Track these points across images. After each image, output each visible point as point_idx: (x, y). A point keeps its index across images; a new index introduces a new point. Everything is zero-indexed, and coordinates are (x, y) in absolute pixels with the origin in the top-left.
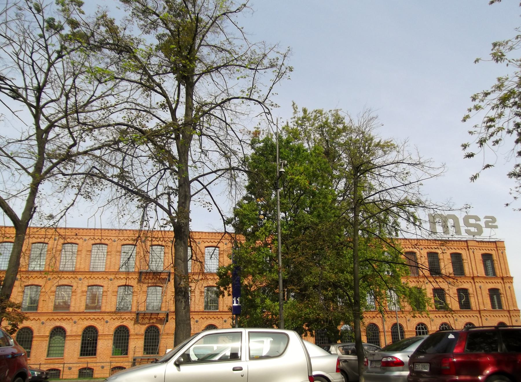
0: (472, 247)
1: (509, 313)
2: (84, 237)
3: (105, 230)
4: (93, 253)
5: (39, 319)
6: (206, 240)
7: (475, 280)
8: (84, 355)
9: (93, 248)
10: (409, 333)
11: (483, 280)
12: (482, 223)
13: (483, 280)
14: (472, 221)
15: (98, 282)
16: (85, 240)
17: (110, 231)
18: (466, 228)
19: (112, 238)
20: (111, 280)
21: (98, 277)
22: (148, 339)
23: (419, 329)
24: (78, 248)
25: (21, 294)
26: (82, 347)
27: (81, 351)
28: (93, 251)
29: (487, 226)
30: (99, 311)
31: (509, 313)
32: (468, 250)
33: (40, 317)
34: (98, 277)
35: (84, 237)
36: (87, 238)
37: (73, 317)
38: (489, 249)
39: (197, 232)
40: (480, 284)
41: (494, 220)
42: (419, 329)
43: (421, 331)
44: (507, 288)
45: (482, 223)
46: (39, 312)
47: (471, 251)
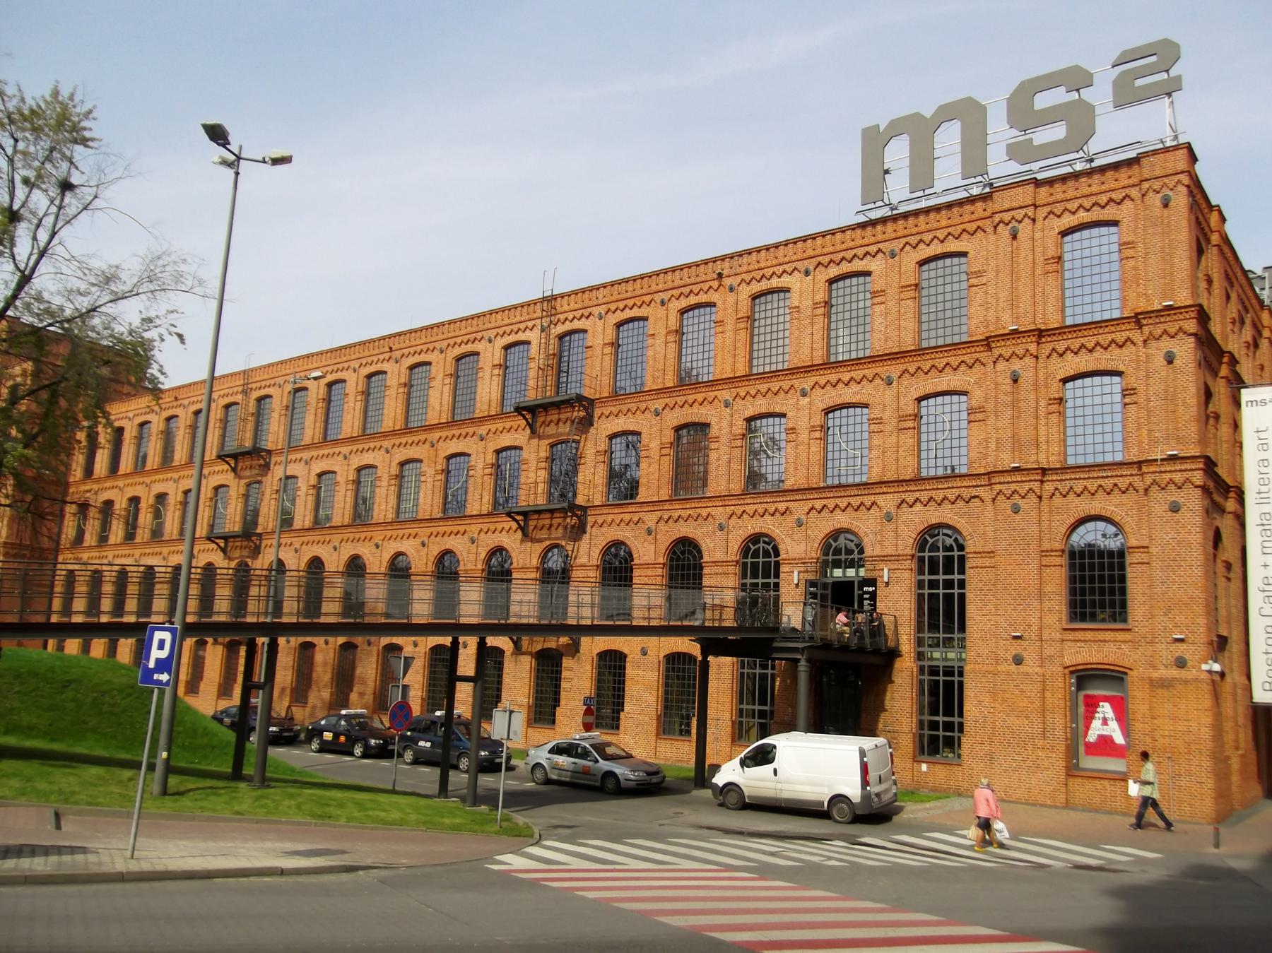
29: (1126, 96)
36: (810, 264)
41: (1166, 53)
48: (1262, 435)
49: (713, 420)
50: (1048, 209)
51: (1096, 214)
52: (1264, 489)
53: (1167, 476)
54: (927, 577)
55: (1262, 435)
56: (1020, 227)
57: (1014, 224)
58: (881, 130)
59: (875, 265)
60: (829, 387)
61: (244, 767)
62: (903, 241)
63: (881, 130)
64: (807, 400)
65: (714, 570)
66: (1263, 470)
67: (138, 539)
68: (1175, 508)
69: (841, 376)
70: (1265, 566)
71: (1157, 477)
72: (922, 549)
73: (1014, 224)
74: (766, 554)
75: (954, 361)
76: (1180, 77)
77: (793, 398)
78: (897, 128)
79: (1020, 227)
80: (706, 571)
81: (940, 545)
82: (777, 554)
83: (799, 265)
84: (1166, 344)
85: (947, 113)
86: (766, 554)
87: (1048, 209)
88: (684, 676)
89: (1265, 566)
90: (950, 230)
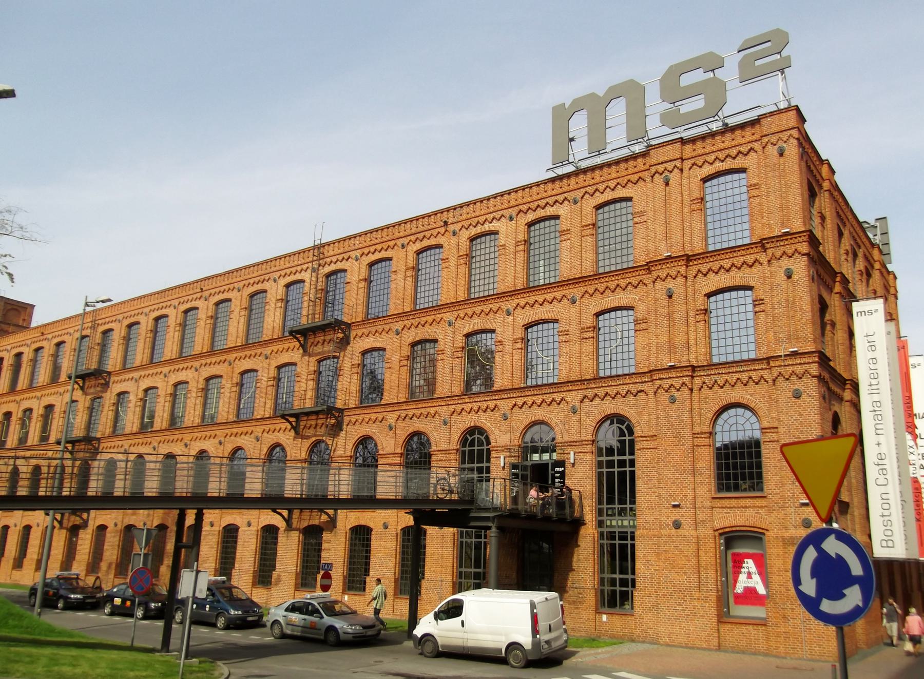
2: (353, 254)
3: (329, 244)
4: (709, 205)
5: (562, 399)
8: (728, 489)
9: (708, 191)
10: (440, 457)
12: (729, 73)
15: (621, 299)
16: (575, 202)
17: (458, 211)
19: (742, 149)
21: (722, 267)
23: (472, 444)
24: (748, 178)
25: (590, 334)
26: (759, 466)
27: (719, 477)
28: (708, 198)
33: (498, 402)
34: (722, 267)
36: (513, 212)
37: (567, 396)
48: (870, 339)
49: (440, 337)
55: (870, 339)
56: (671, 176)
57: (666, 173)
62: (583, 190)
64: (511, 318)
73: (666, 173)
78: (578, 106)
79: (671, 176)
83: (505, 213)
84: (785, 263)
85: (615, 93)
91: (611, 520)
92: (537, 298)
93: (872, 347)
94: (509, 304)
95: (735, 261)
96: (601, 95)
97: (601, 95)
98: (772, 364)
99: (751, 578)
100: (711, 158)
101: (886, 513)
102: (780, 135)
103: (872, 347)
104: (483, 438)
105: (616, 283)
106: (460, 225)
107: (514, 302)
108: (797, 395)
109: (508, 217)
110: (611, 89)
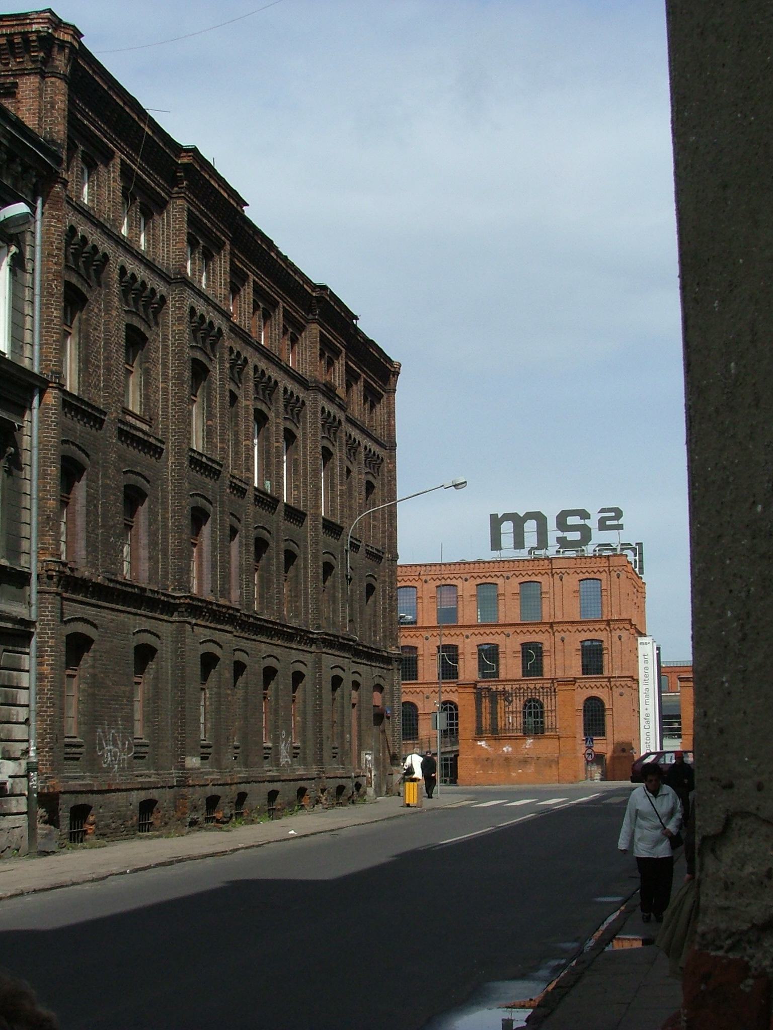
0: (558, 571)
1: (610, 682)
6: (407, 578)
7: (555, 628)
11: (570, 628)
12: (593, 523)
13: (570, 628)
14: (572, 520)
18: (560, 534)
20: (427, 639)
22: (599, 716)
26: (604, 725)
29: (603, 526)
30: (497, 679)
31: (610, 682)
32: (553, 575)
35: (505, 574)
36: (468, 576)
38: (596, 570)
39: (413, 565)
40: (563, 634)
41: (618, 513)
42: (530, 708)
43: (533, 710)
44: (616, 639)
45: (593, 523)
46: (501, 679)
47: (614, 574)
48: (646, 657)
49: (419, 646)
50: (574, 570)
51: (592, 576)
52: (647, 679)
53: (619, 683)
54: (455, 727)
55: (646, 657)
56: (564, 576)
57: (561, 574)
58: (499, 516)
59: (500, 581)
60: (479, 635)
61: (421, 761)
62: (513, 573)
63: (499, 516)
64: (469, 640)
65: (425, 717)
66: (646, 671)
67: (518, 704)
68: (621, 695)
69: (486, 631)
70: (647, 709)
71: (479, 574)
72: (525, 708)
73: (561, 574)
74: (535, 707)
75: (537, 630)
76: (622, 525)
77: (461, 638)
78: (507, 517)
79: (564, 576)
80: (420, 717)
81: (532, 706)
82: (542, 707)
83: (462, 576)
84: (618, 632)
85: (530, 516)
86: (535, 707)
87: (574, 570)
88: (596, 714)
89: (647, 709)
90: (534, 571)
91: (27, 722)
92: (486, 631)
93: (646, 662)
94: (468, 632)
95: (595, 627)
96: (522, 516)
97: (522, 516)
98: (611, 680)
99: (432, 798)
100: (584, 570)
101: (648, 742)
102: (619, 568)
103: (646, 662)
104: (453, 707)
105: (533, 629)
106: (430, 577)
107: (472, 631)
108: (621, 695)
109: (464, 578)
110: (527, 513)
